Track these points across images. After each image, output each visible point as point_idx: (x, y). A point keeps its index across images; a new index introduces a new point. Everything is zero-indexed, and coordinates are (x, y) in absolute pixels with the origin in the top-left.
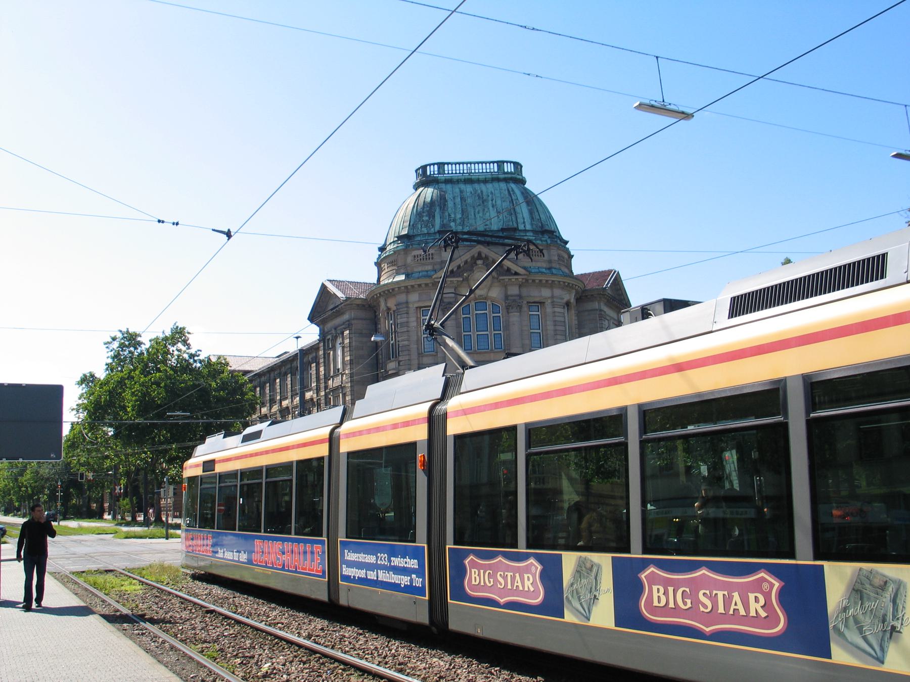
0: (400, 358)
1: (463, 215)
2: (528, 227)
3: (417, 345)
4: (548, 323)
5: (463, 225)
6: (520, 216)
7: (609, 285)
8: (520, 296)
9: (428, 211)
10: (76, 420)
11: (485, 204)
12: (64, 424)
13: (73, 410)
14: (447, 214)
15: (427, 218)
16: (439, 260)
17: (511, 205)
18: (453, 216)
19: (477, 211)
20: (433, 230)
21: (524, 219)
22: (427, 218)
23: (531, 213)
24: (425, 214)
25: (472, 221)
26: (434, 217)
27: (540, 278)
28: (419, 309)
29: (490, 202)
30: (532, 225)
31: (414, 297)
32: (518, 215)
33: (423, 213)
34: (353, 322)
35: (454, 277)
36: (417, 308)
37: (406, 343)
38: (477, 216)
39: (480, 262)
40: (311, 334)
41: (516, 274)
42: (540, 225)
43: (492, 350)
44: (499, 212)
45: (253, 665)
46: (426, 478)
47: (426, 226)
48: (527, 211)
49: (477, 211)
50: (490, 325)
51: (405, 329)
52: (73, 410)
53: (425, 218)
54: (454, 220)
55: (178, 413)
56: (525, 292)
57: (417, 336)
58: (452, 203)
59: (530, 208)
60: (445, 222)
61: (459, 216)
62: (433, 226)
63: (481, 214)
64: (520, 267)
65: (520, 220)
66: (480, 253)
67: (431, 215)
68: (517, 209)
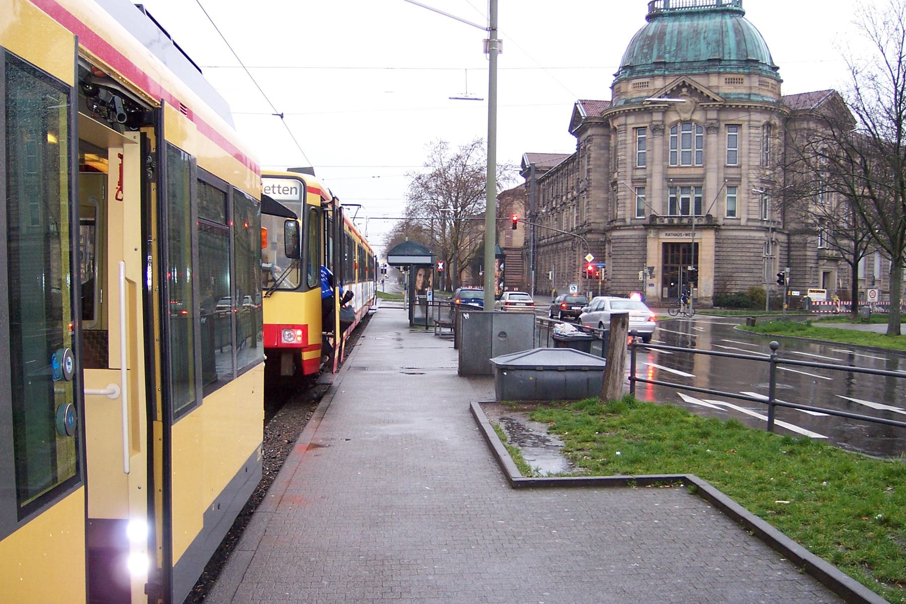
0: (619, 171)
1: (677, 47)
2: (733, 57)
3: (632, 159)
4: (744, 142)
5: (676, 56)
6: (726, 47)
8: (718, 120)
9: (648, 44)
10: (316, 389)
11: (698, 36)
12: (161, 419)
13: (540, 469)
14: (663, 47)
16: (653, 88)
17: (721, 36)
18: (668, 48)
19: (690, 43)
20: (650, 61)
21: (730, 49)
23: (738, 43)
24: (645, 47)
26: (652, 50)
27: (737, 104)
28: (635, 130)
29: (703, 35)
30: (737, 54)
31: (631, 120)
36: (633, 128)
37: (623, 157)
38: (690, 48)
39: (684, 90)
40: (568, 145)
41: (714, 100)
42: (746, 54)
43: (693, 165)
44: (709, 44)
46: (102, 147)
47: (645, 57)
48: (734, 42)
49: (690, 43)
50: (679, 155)
51: (623, 146)
52: (540, 469)
54: (669, 52)
56: (723, 116)
57: (632, 151)
58: (670, 36)
59: (738, 39)
60: (660, 54)
61: (674, 48)
62: (651, 57)
64: (714, 93)
65: (726, 51)
66: (684, 82)
67: (650, 48)
68: (726, 40)
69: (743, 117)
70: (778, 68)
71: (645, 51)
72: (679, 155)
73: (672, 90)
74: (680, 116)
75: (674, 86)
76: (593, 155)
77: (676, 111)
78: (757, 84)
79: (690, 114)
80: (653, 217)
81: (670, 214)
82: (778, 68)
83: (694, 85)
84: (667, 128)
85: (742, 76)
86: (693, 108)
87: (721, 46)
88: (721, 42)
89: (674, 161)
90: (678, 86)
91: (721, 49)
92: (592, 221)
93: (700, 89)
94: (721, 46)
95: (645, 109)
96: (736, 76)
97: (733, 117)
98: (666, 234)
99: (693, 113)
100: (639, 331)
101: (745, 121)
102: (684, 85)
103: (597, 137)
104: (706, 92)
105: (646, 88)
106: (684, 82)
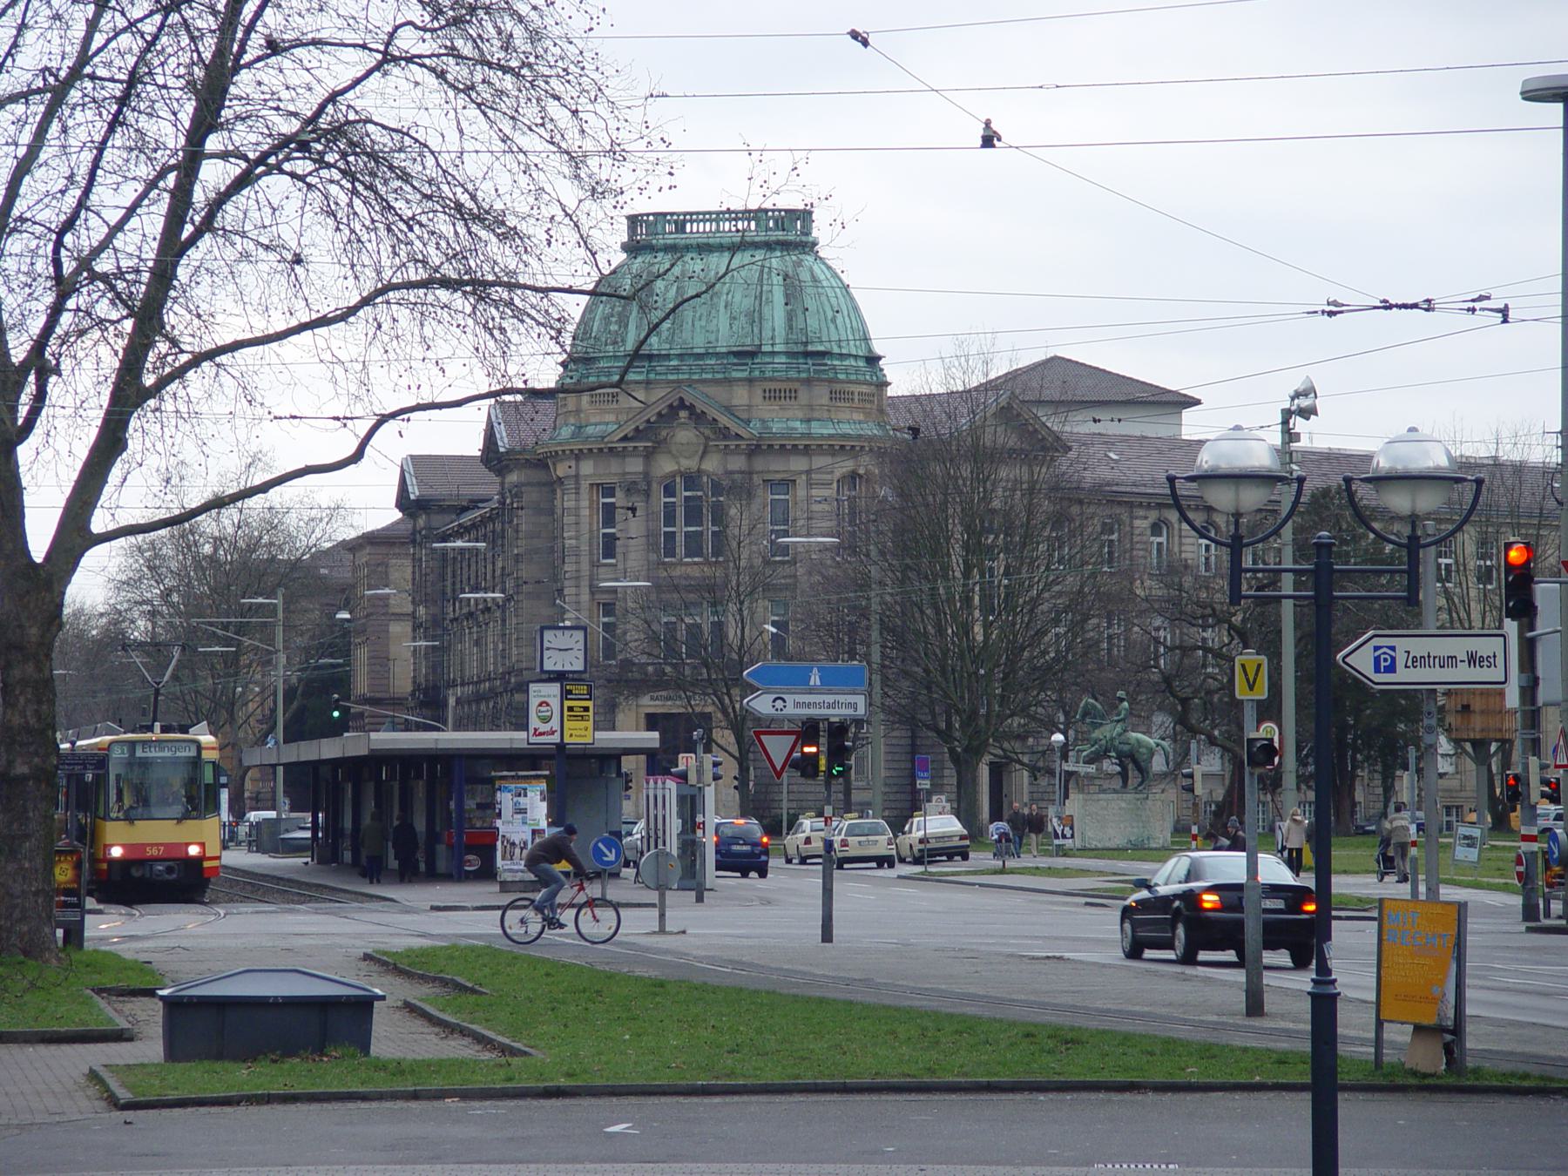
6: (767, 326)
7: (696, 559)
9: (619, 314)
15: (616, 328)
21: (774, 330)
22: (616, 328)
23: (790, 317)
24: (614, 319)
25: (686, 335)
26: (626, 326)
31: (587, 467)
32: (763, 323)
33: (612, 316)
34: (523, 489)
35: (641, 440)
36: (592, 485)
38: (697, 324)
39: (683, 414)
44: (735, 318)
45: (1262, 797)
50: (680, 540)
53: (614, 327)
55: (217, 649)
56: (759, 463)
63: (703, 323)
65: (767, 334)
68: (766, 310)
69: (798, 464)
70: (879, 358)
71: (614, 327)
72: (680, 540)
73: (659, 414)
74: (678, 463)
75: (662, 407)
76: (523, 527)
77: (670, 452)
78: (825, 400)
79: (697, 459)
80: (627, 664)
81: (1295, 562)
82: (879, 358)
83: (700, 407)
84: (655, 485)
85: (796, 385)
86: (702, 448)
87: (757, 323)
88: (756, 314)
89: (670, 552)
90: (671, 406)
91: (756, 330)
92: (524, 665)
93: (712, 413)
94: (757, 323)
95: (611, 449)
96: (783, 386)
97: (778, 466)
98: (652, 699)
99: (702, 458)
100: (695, 953)
101: (801, 473)
102: (682, 404)
103: (529, 488)
104: (724, 420)
105: (615, 406)
106: (681, 399)
